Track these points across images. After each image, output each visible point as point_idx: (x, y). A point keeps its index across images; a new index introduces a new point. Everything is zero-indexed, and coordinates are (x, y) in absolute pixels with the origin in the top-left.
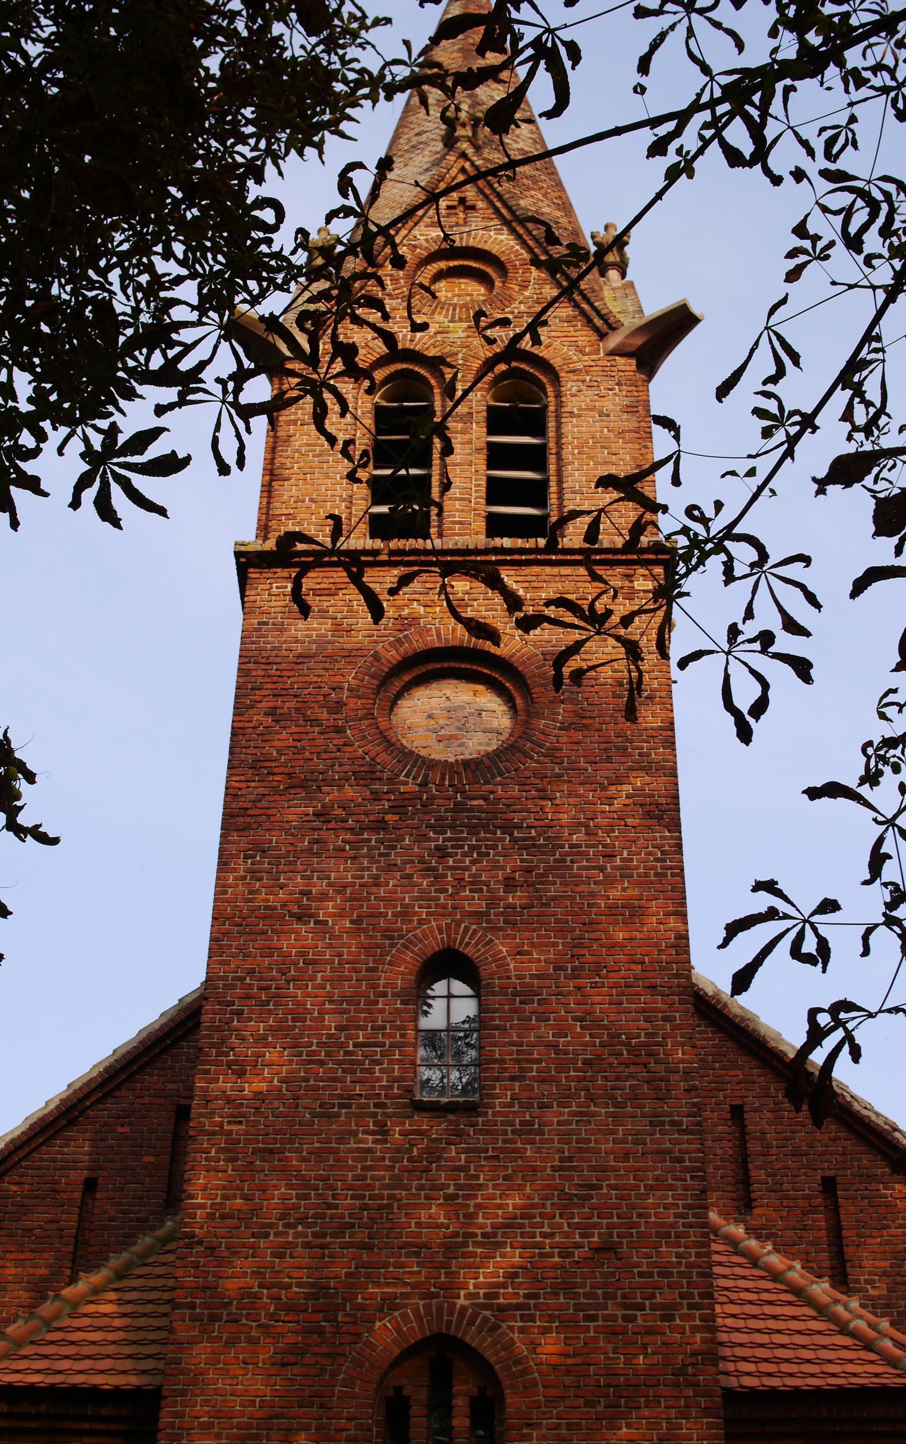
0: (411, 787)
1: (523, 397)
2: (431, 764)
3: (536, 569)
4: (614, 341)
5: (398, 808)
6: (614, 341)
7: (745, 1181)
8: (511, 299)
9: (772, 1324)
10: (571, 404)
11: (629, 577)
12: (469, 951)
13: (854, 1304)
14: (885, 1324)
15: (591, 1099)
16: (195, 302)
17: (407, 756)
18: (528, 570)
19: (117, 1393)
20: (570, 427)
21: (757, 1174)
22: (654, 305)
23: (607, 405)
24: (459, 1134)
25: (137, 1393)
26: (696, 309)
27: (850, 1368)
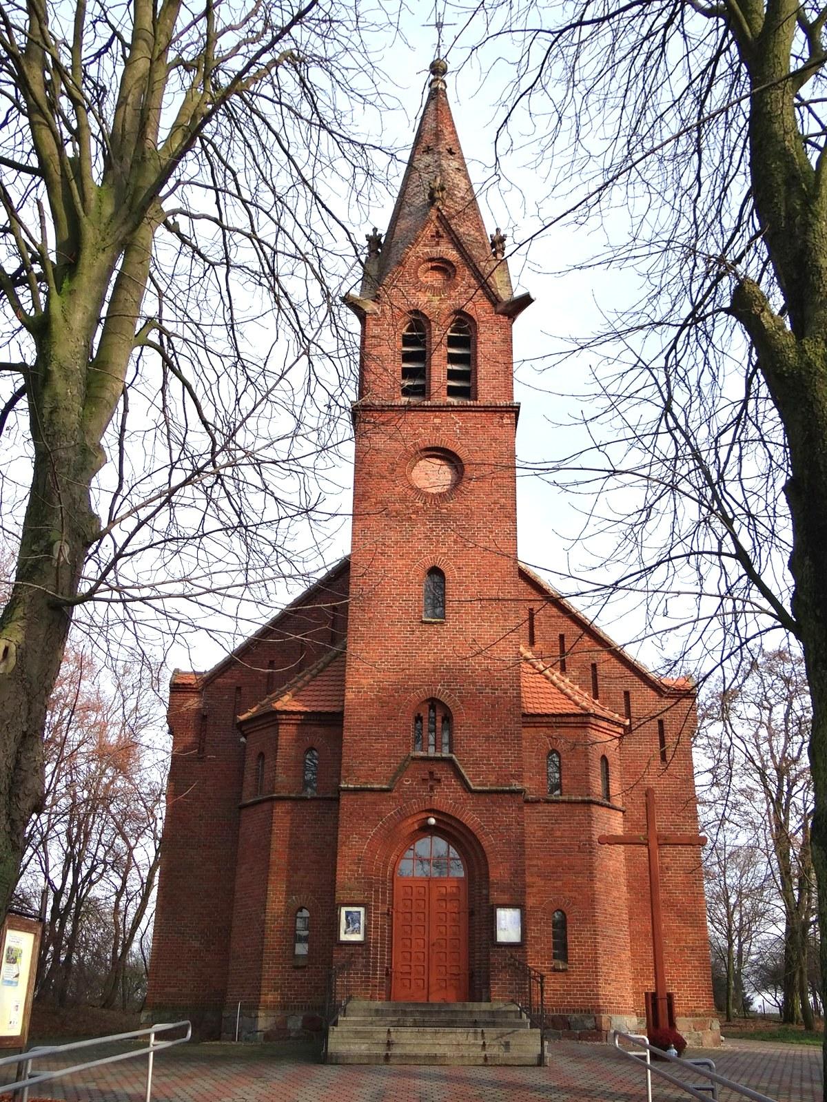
0: (420, 504)
1: (464, 332)
2: (427, 495)
3: (467, 414)
4: (500, 308)
5: (415, 512)
6: (500, 308)
7: (532, 635)
8: (458, 285)
9: (539, 690)
10: (481, 338)
11: (502, 418)
12: (441, 568)
13: (567, 680)
14: (577, 687)
15: (482, 620)
16: (108, 536)
17: (418, 491)
18: (463, 414)
19: (327, 713)
20: (480, 348)
21: (536, 632)
22: (518, 293)
23: (496, 339)
24: (438, 632)
25: (333, 713)
26: (533, 297)
27: (564, 706)
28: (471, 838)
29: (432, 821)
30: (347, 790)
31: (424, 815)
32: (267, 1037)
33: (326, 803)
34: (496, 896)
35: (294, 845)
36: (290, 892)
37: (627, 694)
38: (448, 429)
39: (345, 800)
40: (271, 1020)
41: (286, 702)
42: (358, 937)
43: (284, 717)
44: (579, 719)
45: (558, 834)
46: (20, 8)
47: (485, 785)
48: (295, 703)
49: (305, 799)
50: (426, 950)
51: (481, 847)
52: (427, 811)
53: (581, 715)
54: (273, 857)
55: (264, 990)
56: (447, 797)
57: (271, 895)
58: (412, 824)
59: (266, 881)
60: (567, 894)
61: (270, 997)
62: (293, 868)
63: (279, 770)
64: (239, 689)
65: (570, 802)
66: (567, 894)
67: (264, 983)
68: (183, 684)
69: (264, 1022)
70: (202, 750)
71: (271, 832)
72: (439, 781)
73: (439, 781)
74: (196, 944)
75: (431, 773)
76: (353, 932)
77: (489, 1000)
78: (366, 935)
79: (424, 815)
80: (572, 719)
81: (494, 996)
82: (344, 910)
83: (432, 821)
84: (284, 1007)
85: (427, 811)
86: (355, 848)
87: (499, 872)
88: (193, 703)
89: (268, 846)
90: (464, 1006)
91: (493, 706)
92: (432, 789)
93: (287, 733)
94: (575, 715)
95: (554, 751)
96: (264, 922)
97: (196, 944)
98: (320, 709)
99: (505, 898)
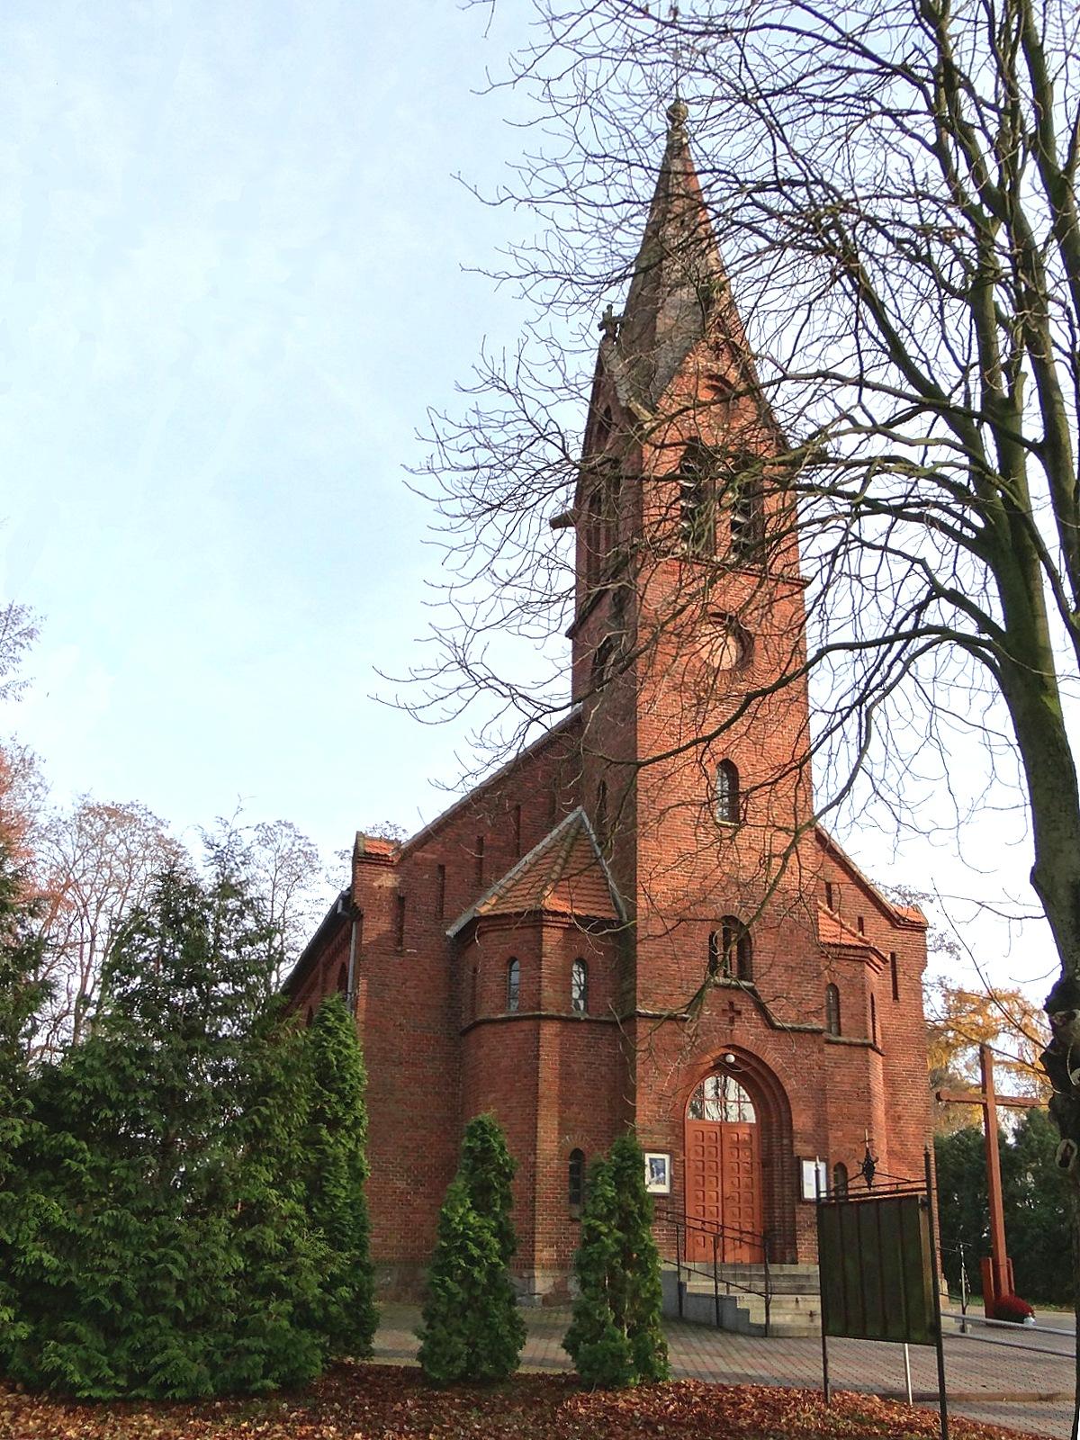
28: (770, 1080)
29: (732, 1058)
30: (646, 1016)
31: (723, 1051)
32: (546, 1300)
33: (613, 1024)
34: (800, 1148)
35: (566, 1076)
36: (563, 1129)
37: (861, 919)
38: (735, 592)
39: (642, 1028)
40: (550, 1282)
41: (552, 902)
42: (663, 1189)
43: (551, 918)
44: (859, 952)
45: (838, 1079)
46: (892, 131)
47: (786, 1021)
48: (561, 902)
49: (577, 1020)
50: (719, 1205)
51: (784, 1093)
52: (728, 1047)
53: (863, 948)
54: (542, 1088)
55: (538, 1246)
56: (748, 1032)
57: (541, 1133)
58: (709, 1060)
59: (535, 1115)
60: (848, 1146)
61: (545, 1254)
62: (565, 1102)
63: (545, 982)
64: (442, 868)
65: (851, 1045)
66: (848, 1146)
67: (538, 1237)
68: (378, 854)
69: (542, 1283)
70: (400, 942)
71: (537, 1057)
72: (739, 1013)
73: (739, 1013)
74: (401, 1185)
75: (731, 1004)
76: (657, 1182)
77: (795, 1262)
78: (671, 1186)
79: (723, 1051)
80: (852, 951)
81: (801, 1257)
82: (648, 1156)
83: (732, 1058)
84: (562, 1266)
85: (728, 1047)
86: (653, 1086)
87: (802, 1120)
88: (388, 880)
89: (536, 1070)
90: (782, 1269)
91: (792, 931)
92: (732, 1021)
93: (552, 937)
94: (856, 947)
95: (832, 984)
96: (534, 1165)
97: (401, 1185)
98: (593, 913)
99: (809, 1149)
